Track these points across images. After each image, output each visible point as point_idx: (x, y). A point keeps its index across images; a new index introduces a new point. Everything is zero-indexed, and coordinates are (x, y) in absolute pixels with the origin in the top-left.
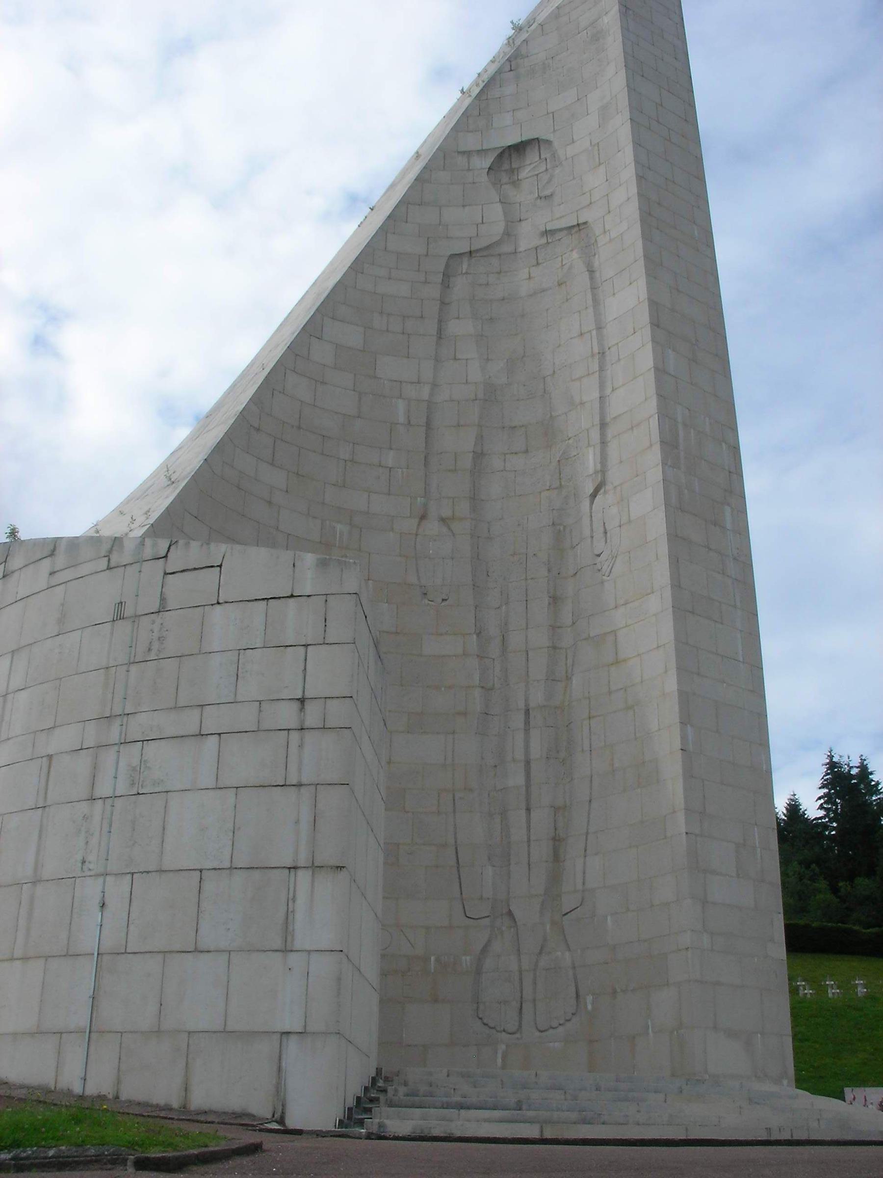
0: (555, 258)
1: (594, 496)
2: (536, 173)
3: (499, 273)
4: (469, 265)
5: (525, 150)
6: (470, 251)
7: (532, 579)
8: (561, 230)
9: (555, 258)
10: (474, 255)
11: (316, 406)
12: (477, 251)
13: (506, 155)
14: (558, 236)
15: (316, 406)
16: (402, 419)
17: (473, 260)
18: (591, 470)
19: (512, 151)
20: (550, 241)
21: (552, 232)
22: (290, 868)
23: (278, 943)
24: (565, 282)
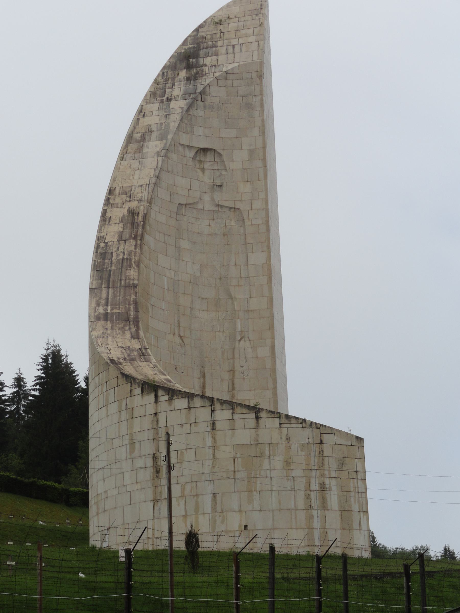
0: (222, 220)
1: (240, 341)
2: (214, 168)
3: (196, 218)
4: (185, 211)
5: (207, 152)
6: (186, 204)
7: (214, 370)
8: (226, 207)
9: (222, 220)
10: (187, 206)
11: (186, 294)
12: (189, 204)
13: (199, 152)
14: (224, 209)
15: (186, 294)
16: (166, 287)
17: (187, 208)
18: (123, 281)
19: (201, 151)
20: (220, 210)
21: (222, 206)
22: (150, 467)
23: (358, 528)
24: (227, 235)
